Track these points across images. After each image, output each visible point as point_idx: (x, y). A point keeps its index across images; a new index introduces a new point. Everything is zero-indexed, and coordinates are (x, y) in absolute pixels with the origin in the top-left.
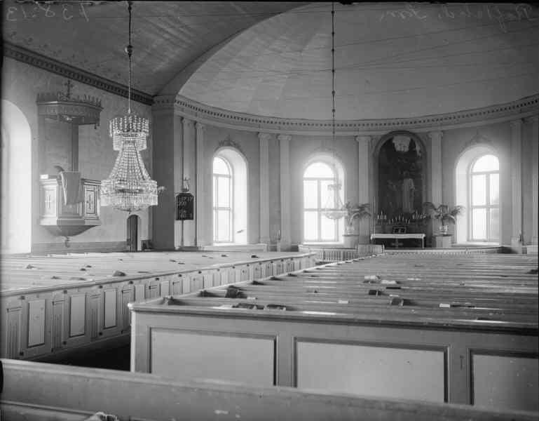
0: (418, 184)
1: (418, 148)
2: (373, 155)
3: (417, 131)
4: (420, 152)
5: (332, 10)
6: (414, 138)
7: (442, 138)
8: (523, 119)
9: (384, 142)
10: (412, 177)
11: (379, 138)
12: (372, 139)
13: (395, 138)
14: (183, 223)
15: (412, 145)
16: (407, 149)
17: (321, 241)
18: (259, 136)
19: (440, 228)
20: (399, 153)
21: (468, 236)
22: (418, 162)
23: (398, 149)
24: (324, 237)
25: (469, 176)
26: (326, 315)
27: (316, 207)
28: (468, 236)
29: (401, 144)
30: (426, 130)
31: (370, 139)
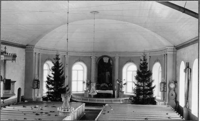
0: (111, 74)
1: (111, 62)
2: (97, 63)
3: (110, 56)
4: (112, 63)
5: (67, 12)
6: (110, 59)
7: (119, 59)
8: (150, 56)
9: (99, 60)
10: (109, 71)
11: (99, 57)
12: (96, 58)
13: (104, 58)
14: (77, 89)
15: (109, 60)
16: (107, 62)
17: (78, 92)
18: (91, 58)
19: (121, 89)
20: (105, 63)
21: (126, 91)
22: (111, 67)
23: (105, 61)
24: (78, 90)
25: (127, 71)
26: (178, 119)
27: (78, 80)
28: (126, 91)
29: (106, 60)
30: (113, 56)
31: (95, 58)
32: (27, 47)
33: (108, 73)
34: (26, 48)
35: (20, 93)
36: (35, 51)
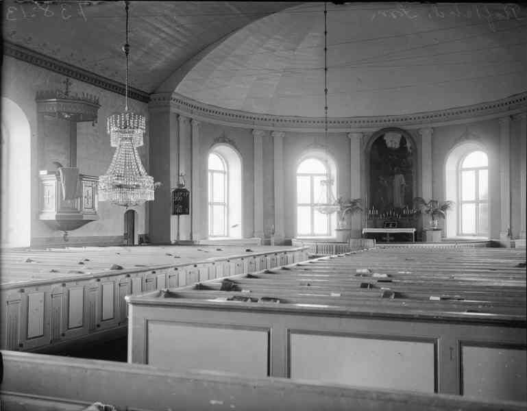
0: (409, 179)
1: (408, 145)
2: (365, 151)
3: (407, 128)
6: (405, 135)
8: (511, 116)
9: (375, 139)
10: (403, 173)
11: (371, 134)
12: (364, 136)
13: (387, 134)
15: (403, 141)
16: (398, 146)
17: (314, 236)
20: (390, 149)
21: (458, 230)
22: (409, 158)
23: (389, 145)
24: (316, 232)
27: (309, 202)
28: (458, 230)
29: (392, 141)
30: (416, 127)
31: (361, 135)
32: (152, 97)
33: (169, 381)
34: (151, 100)
35: (148, 224)
36: (173, 110)
